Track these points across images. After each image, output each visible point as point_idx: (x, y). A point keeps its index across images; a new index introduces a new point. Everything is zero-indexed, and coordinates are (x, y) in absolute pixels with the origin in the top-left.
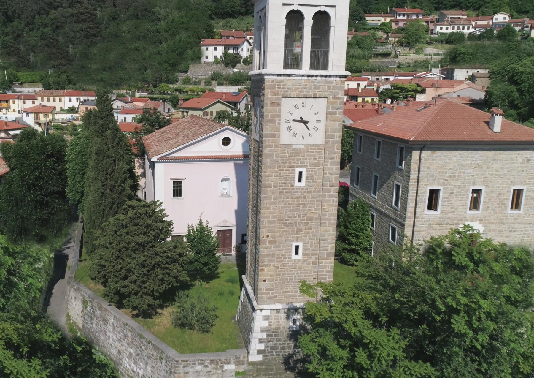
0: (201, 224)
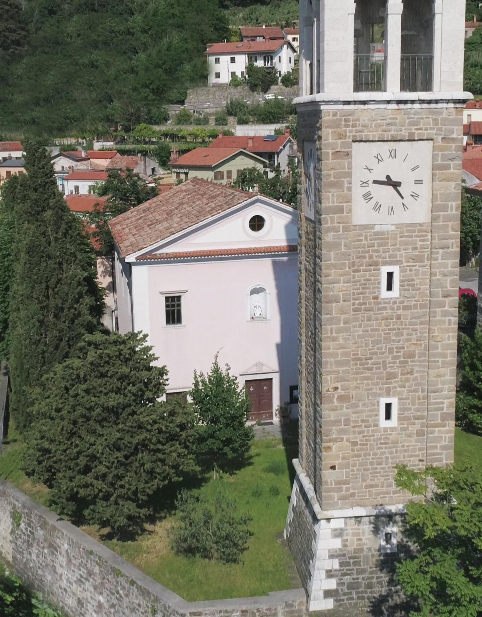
0: (216, 370)
